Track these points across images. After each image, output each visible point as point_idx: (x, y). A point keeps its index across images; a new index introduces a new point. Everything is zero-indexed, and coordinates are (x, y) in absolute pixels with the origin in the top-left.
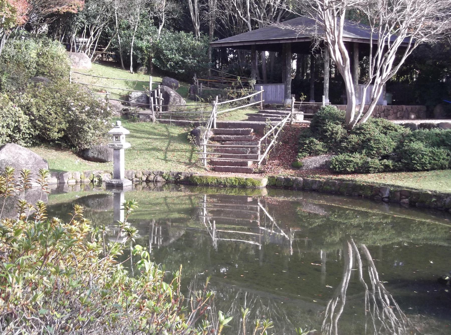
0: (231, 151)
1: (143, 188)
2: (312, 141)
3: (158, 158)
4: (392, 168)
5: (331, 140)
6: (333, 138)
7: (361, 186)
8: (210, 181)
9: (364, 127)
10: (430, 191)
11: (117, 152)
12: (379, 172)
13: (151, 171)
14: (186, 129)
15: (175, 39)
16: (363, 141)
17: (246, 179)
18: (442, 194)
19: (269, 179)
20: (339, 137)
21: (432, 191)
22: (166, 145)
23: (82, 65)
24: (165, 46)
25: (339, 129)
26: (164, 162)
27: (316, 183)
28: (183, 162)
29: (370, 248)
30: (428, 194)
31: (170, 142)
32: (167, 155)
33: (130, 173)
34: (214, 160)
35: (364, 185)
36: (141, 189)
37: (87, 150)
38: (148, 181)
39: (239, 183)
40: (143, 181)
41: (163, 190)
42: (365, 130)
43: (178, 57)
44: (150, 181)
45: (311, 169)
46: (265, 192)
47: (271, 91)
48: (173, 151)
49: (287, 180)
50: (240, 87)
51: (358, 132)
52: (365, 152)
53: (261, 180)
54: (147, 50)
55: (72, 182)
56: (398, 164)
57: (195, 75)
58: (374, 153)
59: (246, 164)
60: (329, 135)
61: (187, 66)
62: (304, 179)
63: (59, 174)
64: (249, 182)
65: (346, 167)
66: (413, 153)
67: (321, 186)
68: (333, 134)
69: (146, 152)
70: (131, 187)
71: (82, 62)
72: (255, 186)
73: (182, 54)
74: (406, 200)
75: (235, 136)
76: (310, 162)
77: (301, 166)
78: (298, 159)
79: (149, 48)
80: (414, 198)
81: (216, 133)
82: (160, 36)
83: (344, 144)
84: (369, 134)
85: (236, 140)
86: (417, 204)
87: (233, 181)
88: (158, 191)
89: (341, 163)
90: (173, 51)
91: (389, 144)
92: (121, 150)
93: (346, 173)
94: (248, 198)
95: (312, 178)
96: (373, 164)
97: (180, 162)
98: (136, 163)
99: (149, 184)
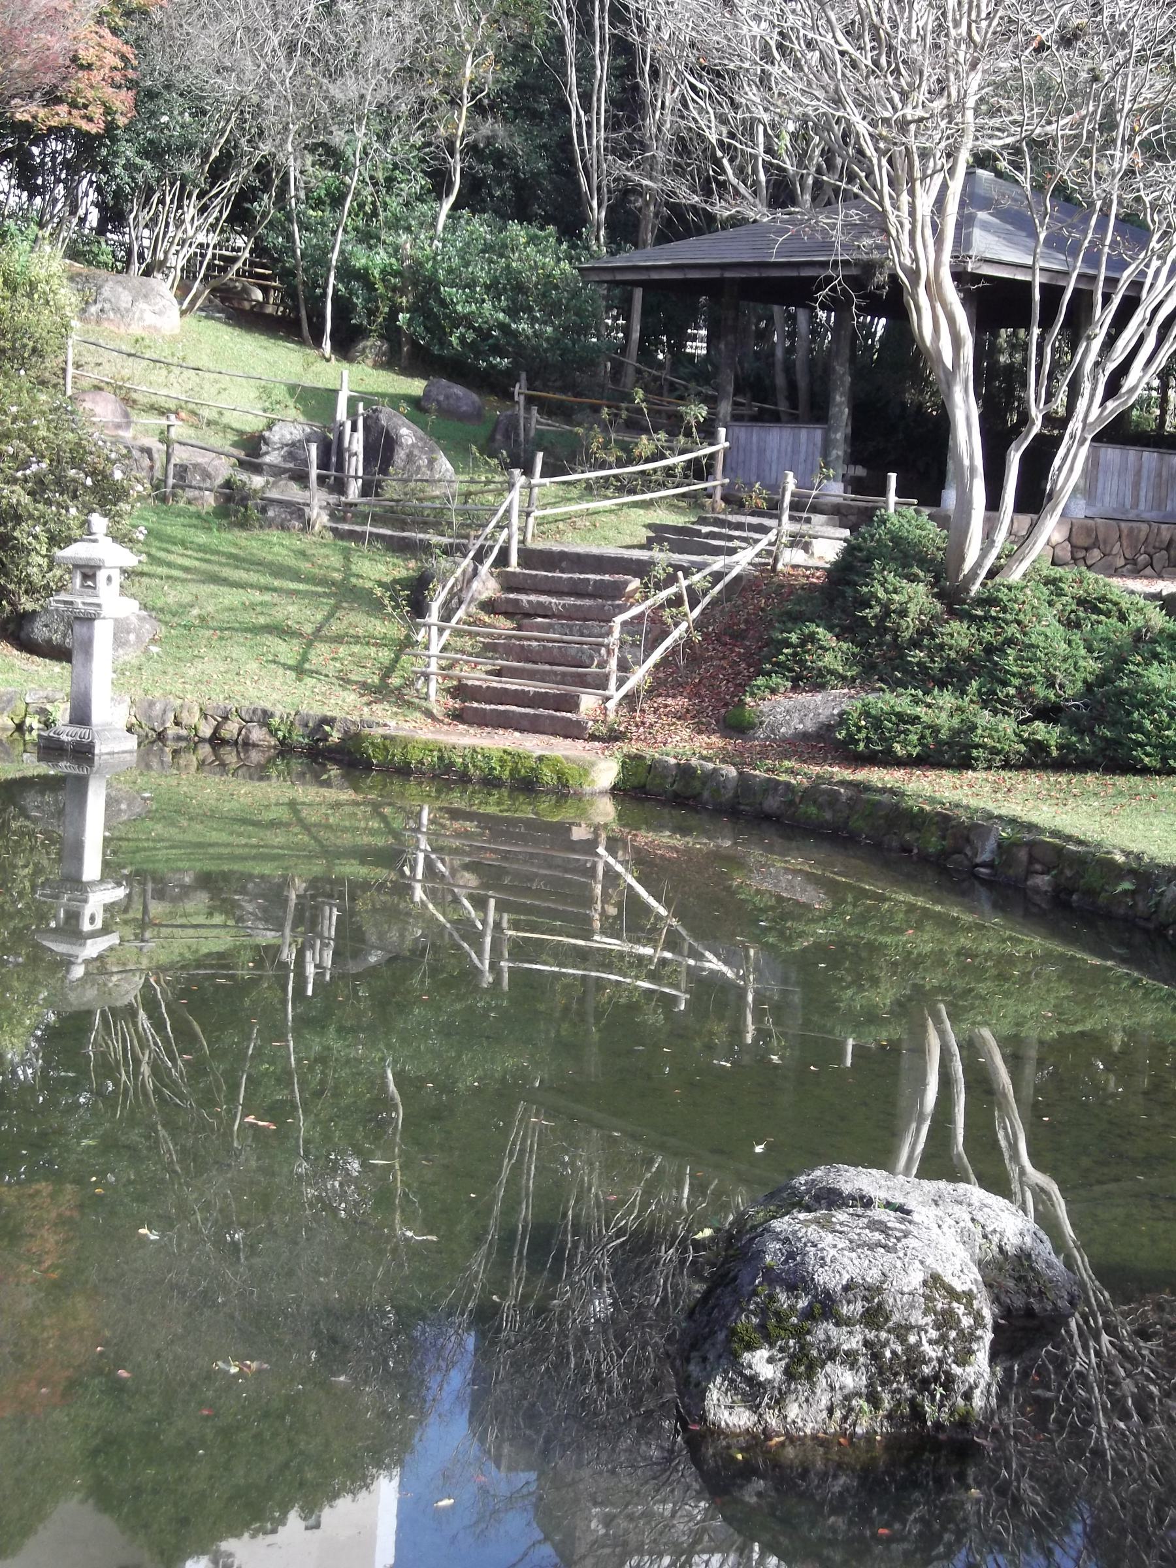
0: (538, 652)
1: (201, 764)
2: (812, 638)
3: (274, 662)
4: (1055, 753)
5: (882, 636)
6: (886, 629)
7: (915, 816)
8: (414, 756)
9: (1004, 595)
10: (1123, 851)
11: (85, 630)
12: (1007, 766)
13: (232, 705)
14: (412, 564)
15: (488, 248)
16: (990, 650)
17: (540, 759)
18: (1158, 866)
20: (909, 626)
21: (1127, 854)
22: (319, 617)
23: (141, 319)
24: (450, 271)
25: (916, 598)
26: (291, 675)
27: (776, 790)
28: (357, 682)
29: (1002, 1042)
30: (1112, 862)
31: (337, 607)
32: (312, 655)
33: (158, 707)
34: (470, 683)
35: (922, 810)
36: (193, 769)
37: (31, 616)
38: (217, 741)
39: (514, 771)
40: (202, 740)
41: (269, 778)
42: (1004, 610)
43: (491, 312)
44: (225, 742)
45: (784, 740)
46: (606, 810)
47: (779, 451)
48: (338, 639)
49: (685, 771)
50: (635, 426)
51: (979, 613)
52: (979, 690)
53: (593, 764)
54: (383, 280)
56: (1081, 741)
57: (523, 375)
58: (1007, 695)
59: (572, 704)
60: (875, 617)
61: (519, 345)
62: (741, 773)
64: (546, 771)
65: (893, 739)
66: (1143, 705)
67: (791, 803)
68: (887, 613)
69: (239, 637)
70: (132, 759)
71: (142, 311)
72: (566, 786)
73: (504, 304)
74: (1042, 881)
75: (571, 601)
76: (785, 709)
77: (752, 726)
78: (748, 699)
79: (396, 274)
80: (1068, 873)
81: (510, 584)
82: (439, 235)
83: (917, 655)
84: (1019, 623)
85: (569, 614)
86: (1075, 897)
87: (494, 763)
88: (251, 778)
89: (877, 723)
90: (473, 291)
91: (1065, 659)
92: (96, 623)
93: (888, 760)
94: (574, 829)
95: (768, 770)
96: (991, 736)
97: (349, 681)
98: (191, 672)
99: (222, 751)
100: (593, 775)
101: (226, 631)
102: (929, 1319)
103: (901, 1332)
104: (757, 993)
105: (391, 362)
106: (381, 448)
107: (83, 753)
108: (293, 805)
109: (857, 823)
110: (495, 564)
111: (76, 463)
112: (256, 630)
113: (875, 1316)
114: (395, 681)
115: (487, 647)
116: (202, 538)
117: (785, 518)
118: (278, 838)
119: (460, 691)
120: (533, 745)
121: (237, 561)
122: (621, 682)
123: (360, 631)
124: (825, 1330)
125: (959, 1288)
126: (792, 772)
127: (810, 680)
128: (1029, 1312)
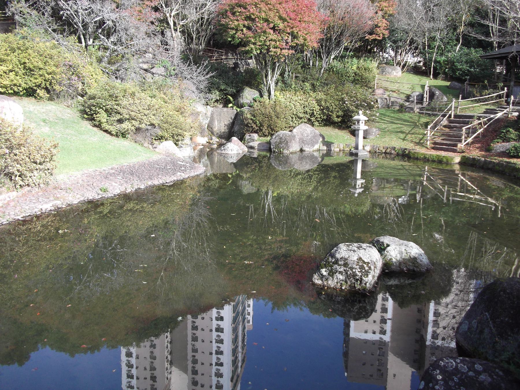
1: (383, 157)
2: (509, 131)
13: (389, 146)
17: (444, 156)
19: (461, 158)
38: (385, 153)
43: (465, 67)
44: (387, 153)
45: (498, 153)
48: (413, 134)
49: (474, 159)
55: (337, 150)
59: (456, 146)
63: (328, 144)
76: (499, 146)
77: (491, 150)
79: (446, 61)
81: (451, 122)
100: (454, 160)
101: (391, 132)
102: (358, 267)
103: (352, 268)
104: (501, 207)
105: (446, 79)
106: (432, 95)
107: (356, 155)
108: (402, 165)
109: (506, 170)
110: (448, 118)
111: (364, 101)
112: (397, 132)
113: (346, 265)
114: (422, 141)
115: (443, 135)
116: (392, 115)
117: (511, 105)
118: (401, 172)
119: (435, 143)
120: (443, 153)
121: (398, 119)
122: (465, 141)
123: (417, 132)
124: (336, 266)
125: (366, 261)
126: (496, 159)
127: (506, 140)
128: (414, 271)
